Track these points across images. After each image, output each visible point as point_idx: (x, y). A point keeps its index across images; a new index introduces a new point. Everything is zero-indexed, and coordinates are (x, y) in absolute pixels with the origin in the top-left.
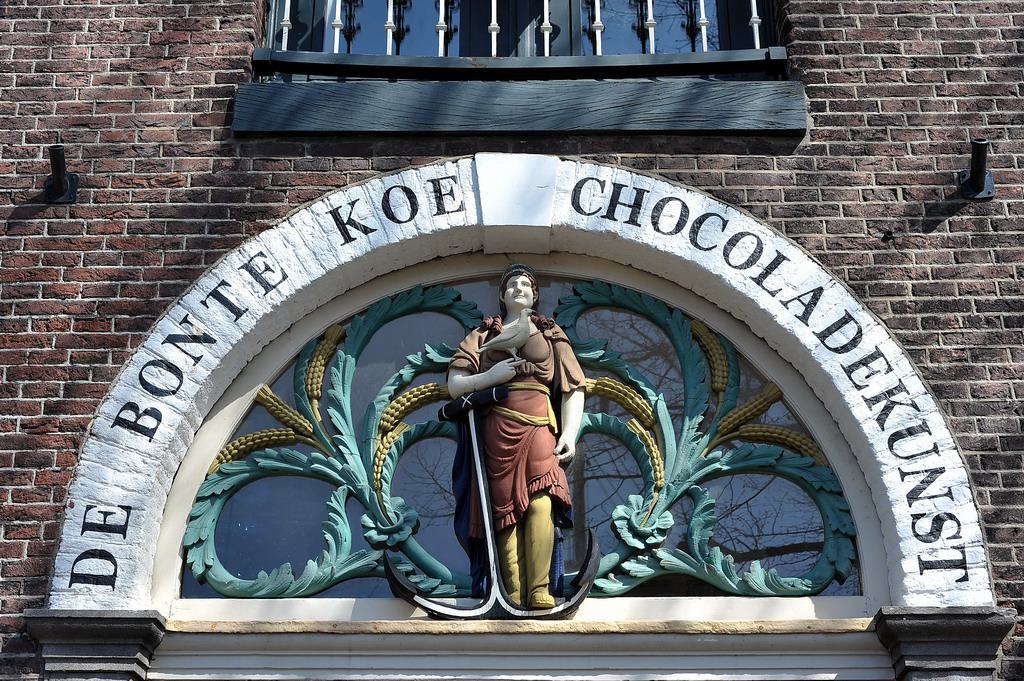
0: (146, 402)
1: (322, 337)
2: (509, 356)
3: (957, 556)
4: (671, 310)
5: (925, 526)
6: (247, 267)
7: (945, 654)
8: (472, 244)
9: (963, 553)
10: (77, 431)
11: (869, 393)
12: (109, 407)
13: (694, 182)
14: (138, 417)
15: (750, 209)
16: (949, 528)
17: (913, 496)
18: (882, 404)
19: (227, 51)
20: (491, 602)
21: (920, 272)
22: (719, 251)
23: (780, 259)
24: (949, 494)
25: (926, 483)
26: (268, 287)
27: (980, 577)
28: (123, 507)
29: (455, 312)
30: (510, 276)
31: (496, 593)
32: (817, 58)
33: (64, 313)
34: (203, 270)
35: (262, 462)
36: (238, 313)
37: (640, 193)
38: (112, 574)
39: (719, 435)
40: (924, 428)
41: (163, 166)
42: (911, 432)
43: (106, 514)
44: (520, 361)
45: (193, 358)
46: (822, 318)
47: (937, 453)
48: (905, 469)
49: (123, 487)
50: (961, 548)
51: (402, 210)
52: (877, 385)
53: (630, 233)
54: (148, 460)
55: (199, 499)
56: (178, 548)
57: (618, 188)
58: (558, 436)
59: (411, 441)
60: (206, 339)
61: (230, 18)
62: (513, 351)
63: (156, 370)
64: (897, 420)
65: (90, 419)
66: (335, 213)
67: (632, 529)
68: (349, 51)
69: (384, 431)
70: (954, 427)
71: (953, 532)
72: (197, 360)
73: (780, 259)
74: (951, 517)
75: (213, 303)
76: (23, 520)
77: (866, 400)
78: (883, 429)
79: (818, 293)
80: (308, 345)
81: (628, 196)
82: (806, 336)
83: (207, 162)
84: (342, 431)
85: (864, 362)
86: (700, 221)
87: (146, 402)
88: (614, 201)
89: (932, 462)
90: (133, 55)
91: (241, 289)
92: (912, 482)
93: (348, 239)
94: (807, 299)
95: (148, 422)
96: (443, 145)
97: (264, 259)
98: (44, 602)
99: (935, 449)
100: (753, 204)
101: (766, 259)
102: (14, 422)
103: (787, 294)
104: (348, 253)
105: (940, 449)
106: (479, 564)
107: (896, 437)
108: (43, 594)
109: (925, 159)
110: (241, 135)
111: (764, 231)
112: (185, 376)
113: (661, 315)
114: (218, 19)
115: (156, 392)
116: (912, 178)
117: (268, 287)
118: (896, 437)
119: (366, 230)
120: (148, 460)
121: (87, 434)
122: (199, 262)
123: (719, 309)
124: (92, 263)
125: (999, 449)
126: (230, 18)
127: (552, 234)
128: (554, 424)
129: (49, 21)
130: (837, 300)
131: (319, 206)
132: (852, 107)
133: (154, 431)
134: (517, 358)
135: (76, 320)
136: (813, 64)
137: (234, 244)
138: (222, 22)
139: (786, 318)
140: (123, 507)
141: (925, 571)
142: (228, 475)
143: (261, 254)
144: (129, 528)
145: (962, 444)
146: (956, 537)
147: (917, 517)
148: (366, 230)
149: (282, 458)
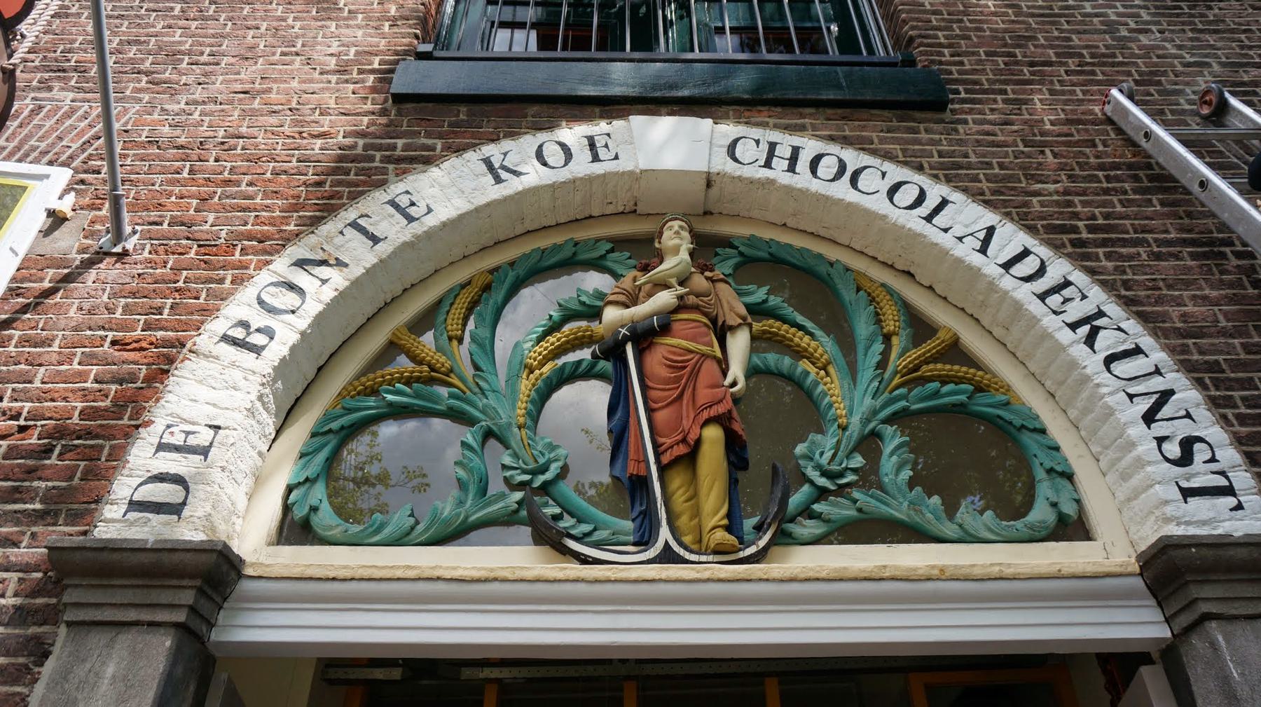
2: (666, 286)
5: (1173, 450)
6: (393, 203)
7: (1232, 596)
9: (1227, 478)
10: (173, 347)
11: (1072, 317)
12: (218, 326)
13: (846, 141)
14: (249, 334)
17: (1149, 418)
19: (392, 44)
20: (660, 545)
21: (1089, 214)
22: (883, 194)
23: (944, 203)
24: (1188, 416)
26: (410, 219)
28: (210, 427)
29: (609, 264)
30: (667, 222)
31: (665, 534)
33: (188, 239)
34: (344, 205)
38: (181, 501)
39: (899, 376)
41: (317, 122)
42: (1127, 354)
43: (188, 433)
44: (682, 290)
45: (321, 280)
47: (1161, 374)
48: (1131, 391)
49: (214, 405)
50: (1222, 473)
52: (1076, 310)
53: (785, 179)
54: (251, 377)
55: (314, 435)
58: (725, 374)
60: (340, 264)
61: (399, 23)
62: (673, 281)
63: (278, 290)
64: (1107, 341)
65: (192, 337)
67: (818, 467)
68: (510, 49)
71: (1208, 456)
72: (324, 282)
73: (944, 203)
74: (1200, 440)
75: (350, 232)
76: (86, 439)
77: (1068, 325)
78: (1095, 352)
79: (991, 231)
81: (784, 151)
82: (991, 269)
83: (361, 121)
84: (485, 369)
87: (259, 319)
89: (1157, 384)
90: (303, 45)
92: (1144, 405)
94: (982, 235)
96: (597, 110)
97: (409, 196)
99: (1157, 372)
100: (908, 159)
102: (104, 338)
103: (958, 230)
104: (495, 192)
105: (1162, 371)
106: (641, 505)
107: (1109, 360)
108: (88, 525)
109: (1065, 129)
110: (399, 99)
112: (308, 296)
114: (387, 24)
115: (272, 310)
116: (1057, 142)
117: (410, 219)
118: (1109, 360)
120: (251, 377)
121: (185, 351)
122: (341, 198)
123: (880, 262)
124: (227, 197)
125: (1228, 371)
126: (399, 23)
127: (709, 184)
128: (719, 354)
129: (230, 23)
130: (1010, 238)
131: (470, 155)
133: (263, 348)
134: (679, 288)
135: (199, 246)
137: (382, 184)
138: (391, 26)
140: (210, 427)
141: (1189, 499)
142: (350, 411)
143: (407, 192)
144: (213, 449)
146: (1213, 460)
147: (1160, 440)
149: (417, 395)
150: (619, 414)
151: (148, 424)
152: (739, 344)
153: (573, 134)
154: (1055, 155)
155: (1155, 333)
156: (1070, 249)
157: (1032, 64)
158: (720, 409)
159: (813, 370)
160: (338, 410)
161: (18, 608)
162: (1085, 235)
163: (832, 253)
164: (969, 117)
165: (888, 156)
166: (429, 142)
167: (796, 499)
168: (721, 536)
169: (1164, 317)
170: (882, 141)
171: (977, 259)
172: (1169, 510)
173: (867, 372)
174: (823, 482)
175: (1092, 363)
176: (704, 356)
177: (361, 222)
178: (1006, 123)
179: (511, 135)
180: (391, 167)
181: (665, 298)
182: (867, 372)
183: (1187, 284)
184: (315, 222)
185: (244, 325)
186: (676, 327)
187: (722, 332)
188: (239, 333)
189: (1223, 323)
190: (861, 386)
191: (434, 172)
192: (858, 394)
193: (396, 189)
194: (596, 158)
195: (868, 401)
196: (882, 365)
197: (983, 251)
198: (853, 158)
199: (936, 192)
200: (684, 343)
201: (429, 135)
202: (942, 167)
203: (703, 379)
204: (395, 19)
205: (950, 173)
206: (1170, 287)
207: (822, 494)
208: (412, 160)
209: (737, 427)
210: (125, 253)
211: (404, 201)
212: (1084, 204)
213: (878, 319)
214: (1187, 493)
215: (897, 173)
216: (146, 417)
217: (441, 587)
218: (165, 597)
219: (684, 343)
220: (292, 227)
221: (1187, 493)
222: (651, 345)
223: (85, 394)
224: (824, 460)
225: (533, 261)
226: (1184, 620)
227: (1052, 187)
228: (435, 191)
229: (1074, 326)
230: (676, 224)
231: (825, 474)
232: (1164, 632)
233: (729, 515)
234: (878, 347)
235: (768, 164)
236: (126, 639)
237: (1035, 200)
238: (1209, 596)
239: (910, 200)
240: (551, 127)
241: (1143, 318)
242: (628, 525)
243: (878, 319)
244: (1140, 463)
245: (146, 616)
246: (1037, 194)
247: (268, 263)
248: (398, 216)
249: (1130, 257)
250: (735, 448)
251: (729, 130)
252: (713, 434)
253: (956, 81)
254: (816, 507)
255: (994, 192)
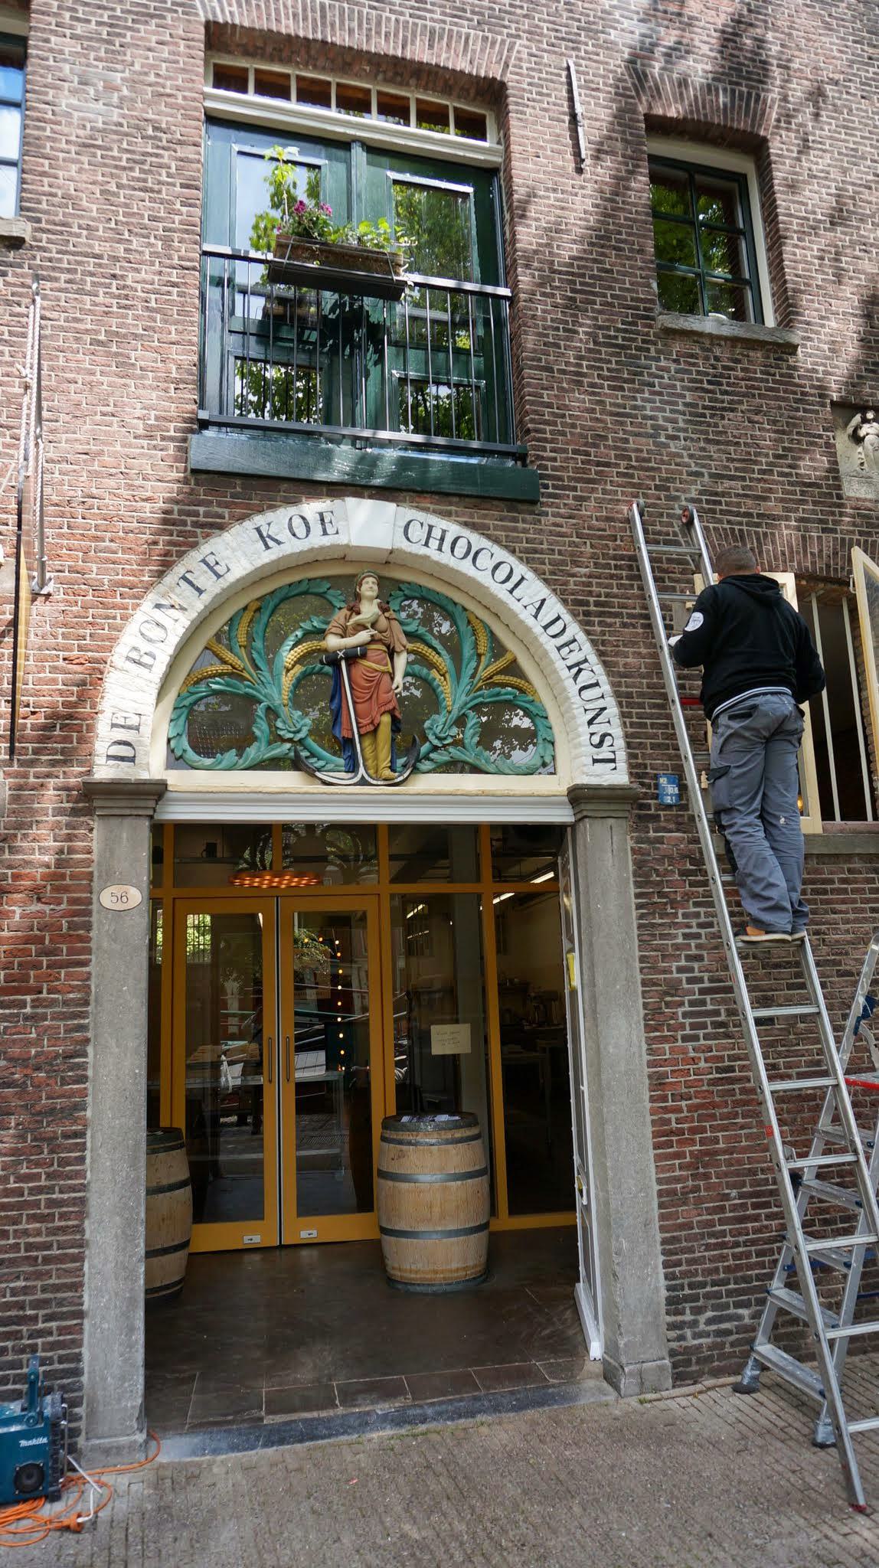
0: (145, 647)
1: (245, 609)
2: (366, 628)
3: (612, 756)
4: (455, 604)
5: (596, 739)
6: (204, 561)
8: (384, 557)
15: (506, 547)
16: (608, 741)
17: (590, 722)
18: (575, 670)
25: (598, 715)
26: (219, 576)
27: (622, 766)
31: (362, 770)
32: (545, 454)
35: (214, 686)
36: (200, 591)
37: (444, 532)
40: (597, 684)
44: (374, 632)
46: (546, 616)
51: (300, 531)
52: (574, 658)
53: (435, 556)
56: (165, 740)
57: (431, 527)
58: (392, 679)
59: (305, 676)
64: (585, 678)
66: (258, 530)
69: (288, 670)
70: (613, 684)
80: (237, 613)
81: (437, 533)
85: (566, 644)
86: (477, 553)
87: (145, 647)
88: (429, 536)
89: (600, 704)
91: (204, 579)
93: (267, 547)
95: (146, 660)
98: (89, 773)
101: (515, 579)
102: (58, 656)
103: (524, 602)
109: (602, 524)
111: (511, 560)
113: (450, 608)
117: (219, 576)
119: (279, 543)
130: (554, 607)
131: (247, 524)
132: (564, 488)
136: (543, 458)
137: (194, 545)
139: (526, 616)
142: (193, 694)
145: (617, 695)
148: (279, 543)
149: (228, 685)
150: (336, 701)
151: (102, 712)
152: (401, 662)
153: (311, 508)
154: (592, 546)
155: (609, 674)
156: (581, 617)
157: (598, 464)
158: (390, 707)
159: (438, 677)
160: (185, 694)
161: (72, 808)
162: (592, 608)
163: (457, 597)
164: (550, 510)
165: (496, 541)
166: (220, 510)
167: (425, 748)
168: (387, 773)
169: (616, 664)
170: (496, 528)
171: (530, 621)
172: (585, 769)
173: (465, 680)
174: (436, 742)
175: (573, 689)
176: (383, 673)
177: (188, 576)
178: (570, 517)
179: (272, 507)
180: (199, 531)
181: (363, 636)
182: (465, 680)
183: (634, 644)
184: (160, 574)
185: (135, 649)
186: (370, 654)
187: (392, 653)
188: (134, 655)
189: (643, 670)
190: (462, 688)
191: (226, 536)
192: (459, 691)
193: (205, 549)
194: (325, 533)
195: (464, 698)
196: (473, 676)
197: (536, 617)
198: (478, 541)
199: (520, 570)
200: (374, 666)
201: (219, 504)
202: (527, 551)
203: (383, 686)
204: (177, 382)
205: (529, 557)
206: (625, 646)
207: (435, 748)
208: (212, 526)
209: (397, 714)
210: (48, 595)
211: (211, 560)
212: (599, 585)
213: (476, 646)
214: (595, 761)
215: (501, 554)
216: (99, 708)
217: (260, 796)
218: (142, 804)
219: (374, 666)
220: (146, 578)
221: (595, 761)
222: (355, 663)
223: (61, 693)
224: (438, 731)
225: (285, 591)
226: (579, 816)
227: (583, 570)
228: (228, 553)
229: (570, 668)
230: (371, 579)
231: (438, 738)
232: (572, 819)
233: (391, 761)
234: (473, 664)
235: (426, 544)
236: (127, 821)
237: (572, 580)
238: (588, 808)
239: (503, 578)
240: (294, 502)
241: (605, 664)
242: (342, 761)
243: (476, 646)
244: (580, 745)
245: (128, 812)
246: (573, 575)
247: (138, 605)
248: (210, 573)
249: (610, 625)
250: (395, 723)
251: (407, 513)
252: (386, 719)
253: (548, 477)
254: (432, 755)
255: (553, 573)
